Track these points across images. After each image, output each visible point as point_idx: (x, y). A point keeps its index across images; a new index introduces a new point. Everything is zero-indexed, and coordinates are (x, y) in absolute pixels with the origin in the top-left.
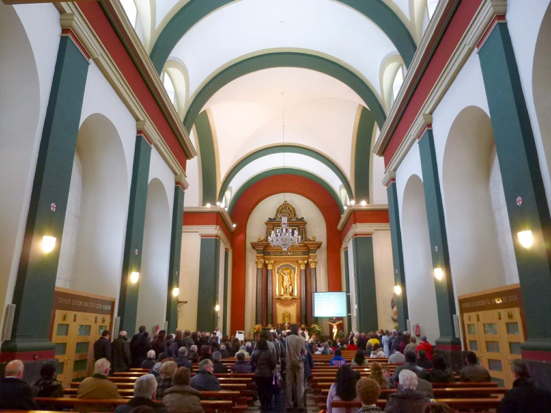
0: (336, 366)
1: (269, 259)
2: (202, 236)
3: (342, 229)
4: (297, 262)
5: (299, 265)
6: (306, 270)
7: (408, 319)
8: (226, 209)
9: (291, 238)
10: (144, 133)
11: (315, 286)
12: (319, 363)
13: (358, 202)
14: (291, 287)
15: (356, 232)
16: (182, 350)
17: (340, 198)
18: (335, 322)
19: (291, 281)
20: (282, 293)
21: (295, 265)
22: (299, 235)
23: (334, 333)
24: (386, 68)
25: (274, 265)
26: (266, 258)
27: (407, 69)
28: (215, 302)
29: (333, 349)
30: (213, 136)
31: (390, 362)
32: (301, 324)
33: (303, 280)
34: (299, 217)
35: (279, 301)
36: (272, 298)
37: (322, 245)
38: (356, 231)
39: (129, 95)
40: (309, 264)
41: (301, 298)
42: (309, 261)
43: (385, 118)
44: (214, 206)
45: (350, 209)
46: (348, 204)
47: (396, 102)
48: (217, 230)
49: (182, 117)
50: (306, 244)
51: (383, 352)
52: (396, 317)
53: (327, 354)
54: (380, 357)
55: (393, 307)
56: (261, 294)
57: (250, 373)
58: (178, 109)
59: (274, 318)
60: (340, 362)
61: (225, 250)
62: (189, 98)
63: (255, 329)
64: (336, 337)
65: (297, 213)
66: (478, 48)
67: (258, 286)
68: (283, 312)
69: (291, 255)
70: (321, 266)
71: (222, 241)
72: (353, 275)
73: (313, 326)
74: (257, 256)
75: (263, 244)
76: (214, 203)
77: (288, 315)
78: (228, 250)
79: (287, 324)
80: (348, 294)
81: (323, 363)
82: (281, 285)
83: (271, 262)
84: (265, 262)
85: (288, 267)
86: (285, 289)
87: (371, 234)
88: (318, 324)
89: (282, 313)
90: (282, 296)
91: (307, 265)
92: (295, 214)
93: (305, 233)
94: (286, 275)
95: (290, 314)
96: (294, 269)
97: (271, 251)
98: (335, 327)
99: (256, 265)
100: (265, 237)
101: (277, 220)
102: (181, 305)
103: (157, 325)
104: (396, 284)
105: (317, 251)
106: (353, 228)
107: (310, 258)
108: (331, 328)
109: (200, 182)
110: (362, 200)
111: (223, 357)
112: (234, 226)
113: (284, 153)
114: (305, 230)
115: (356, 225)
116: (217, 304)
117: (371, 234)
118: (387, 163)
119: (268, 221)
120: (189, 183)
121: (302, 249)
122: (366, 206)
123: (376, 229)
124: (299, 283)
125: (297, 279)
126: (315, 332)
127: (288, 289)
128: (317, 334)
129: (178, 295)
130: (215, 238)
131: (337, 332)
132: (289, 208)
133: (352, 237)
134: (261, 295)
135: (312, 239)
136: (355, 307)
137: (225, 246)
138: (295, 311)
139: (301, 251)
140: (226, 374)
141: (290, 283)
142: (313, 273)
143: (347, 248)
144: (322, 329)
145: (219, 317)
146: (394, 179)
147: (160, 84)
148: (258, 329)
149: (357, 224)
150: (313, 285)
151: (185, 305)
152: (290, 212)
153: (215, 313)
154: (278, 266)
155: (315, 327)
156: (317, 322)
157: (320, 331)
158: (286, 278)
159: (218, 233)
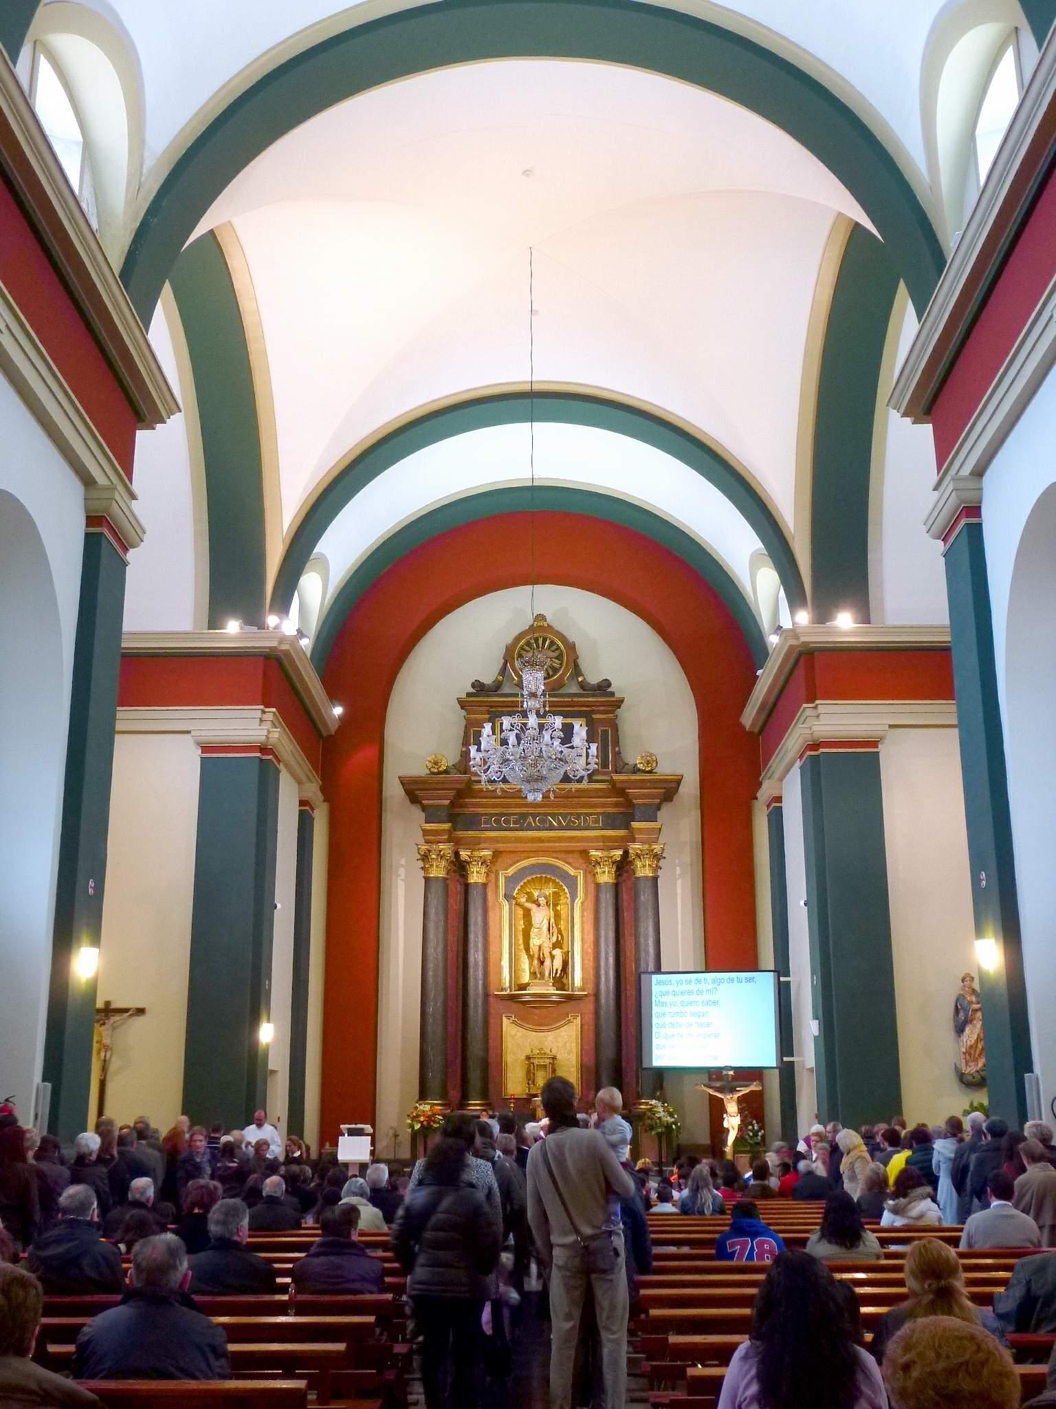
0: (744, 1262)
1: (474, 844)
2: (206, 749)
3: (760, 724)
4: (584, 853)
5: (590, 865)
6: (617, 886)
7: (1031, 1071)
8: (306, 643)
9: (562, 752)
10: (109, 522)
11: (651, 950)
12: (672, 1249)
13: (823, 615)
14: (557, 953)
15: (816, 735)
16: (70, 1196)
17: (753, 607)
18: (733, 1090)
19: (560, 932)
20: (526, 978)
21: (576, 868)
22: (590, 739)
23: (728, 1130)
25: (491, 865)
27: (1040, 46)
28: (255, 1008)
29: (726, 1196)
30: (252, 347)
31: (970, 1245)
33: (607, 924)
34: (593, 679)
35: (514, 1006)
36: (487, 995)
37: (683, 789)
38: (815, 728)
39: (59, 403)
40: (631, 863)
41: (597, 995)
42: (631, 851)
43: (939, 260)
44: (254, 629)
45: (794, 642)
46: (786, 623)
48: (267, 726)
49: (116, 248)
50: (618, 785)
51: (934, 1206)
52: (971, 1069)
53: (702, 1213)
54: (922, 1223)
55: (960, 1030)
56: (440, 980)
57: (371, 1293)
58: (99, 217)
59: (492, 1072)
60: (760, 1245)
61: (424, 835)
62: (145, 171)
64: (736, 1149)
65: (584, 664)
67: (431, 951)
68: (528, 1052)
69: (561, 828)
70: (678, 871)
71: (287, 766)
72: (802, 903)
73: (647, 1104)
74: (425, 832)
75: (452, 782)
76: (253, 618)
77: (548, 1061)
78: (313, 809)
80: (782, 979)
81: (685, 1250)
83: (482, 853)
84: (457, 854)
85: (546, 874)
86: (536, 962)
87: (874, 744)
88: (663, 1100)
90: (523, 987)
91: (623, 866)
92: (576, 666)
93: (616, 742)
94: (539, 905)
95: (554, 1058)
96: (572, 882)
97: (480, 810)
98: (732, 1107)
99: (422, 868)
100: (458, 758)
101: (506, 689)
102: (122, 1024)
103: (7, 1100)
104: (979, 932)
105: (663, 814)
106: (769, 775)
107: (634, 841)
108: (717, 1110)
109: (197, 533)
110: (838, 612)
111: (255, 1228)
112: (338, 711)
113: (538, 426)
115: (815, 708)
116: (264, 1018)
117: (874, 744)
118: (944, 448)
119: (469, 695)
120: (146, 526)
121: (604, 805)
122: (854, 633)
123: (892, 723)
124: (590, 937)
125: (582, 923)
126: (652, 1128)
127: (548, 963)
128: (660, 1135)
129: (97, 974)
130: (258, 755)
131: (740, 1129)
132: (552, 643)
133: (801, 757)
134: (441, 986)
135: (639, 766)
136: (809, 1028)
137: (300, 791)
138: (574, 1045)
139: (599, 810)
140: (267, 1298)
141: (554, 939)
142: (645, 897)
143: (779, 799)
144: (683, 1117)
145: (273, 1072)
146: (974, 510)
147: (19, 100)
148: (430, 1118)
149: (818, 702)
150: (647, 945)
151: (139, 1021)
152: (556, 658)
153: (256, 1053)
156: (661, 1087)
157: (674, 1126)
158: (540, 917)
159: (270, 736)
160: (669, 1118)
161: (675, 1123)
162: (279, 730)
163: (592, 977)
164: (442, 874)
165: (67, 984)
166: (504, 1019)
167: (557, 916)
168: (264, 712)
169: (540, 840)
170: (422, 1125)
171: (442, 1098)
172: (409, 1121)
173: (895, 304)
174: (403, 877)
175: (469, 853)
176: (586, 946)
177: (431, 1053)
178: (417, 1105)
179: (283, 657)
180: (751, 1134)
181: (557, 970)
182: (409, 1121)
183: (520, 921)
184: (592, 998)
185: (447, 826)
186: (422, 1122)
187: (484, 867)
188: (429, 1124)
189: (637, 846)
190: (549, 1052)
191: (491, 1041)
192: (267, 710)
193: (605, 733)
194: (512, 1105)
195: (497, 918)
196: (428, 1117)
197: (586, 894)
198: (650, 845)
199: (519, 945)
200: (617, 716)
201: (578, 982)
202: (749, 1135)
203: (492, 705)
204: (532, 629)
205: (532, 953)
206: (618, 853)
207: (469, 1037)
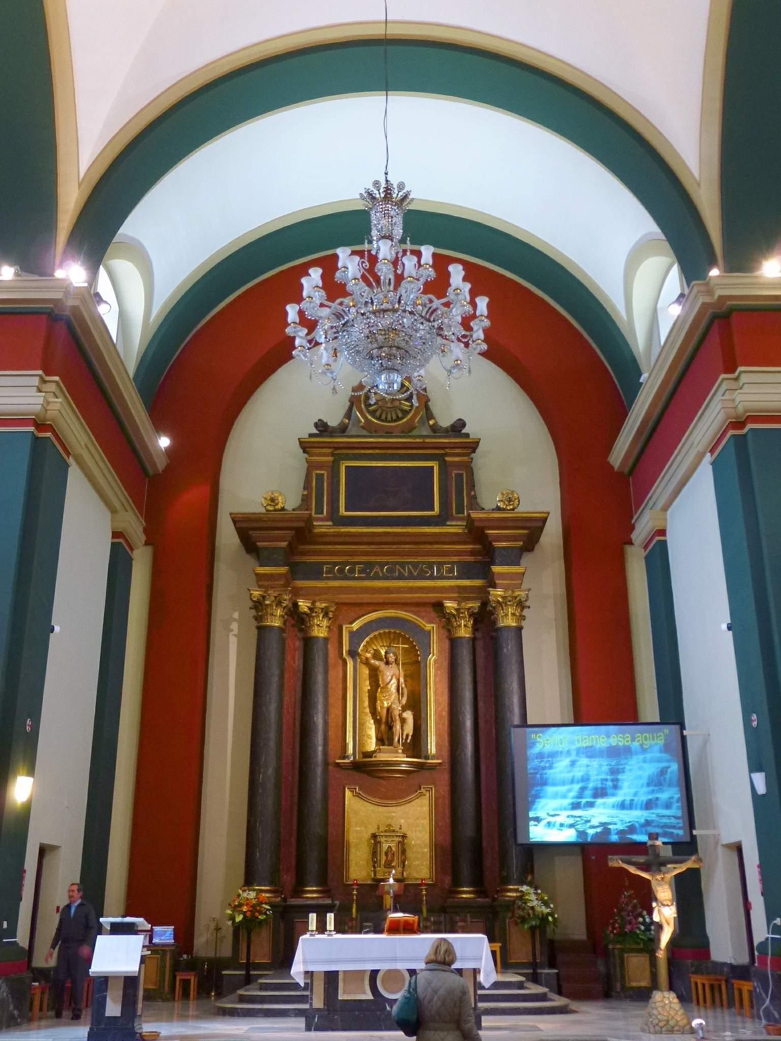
4: (438, 606)
5: (447, 621)
24: (642, 262)
26: (301, 588)
32: (457, 882)
34: (445, 421)
40: (492, 613)
45: (708, 300)
47: (666, 349)
50: (477, 524)
61: (113, 537)
63: (237, 908)
65: (436, 407)
66: (712, 455)
68: (372, 830)
72: (724, 627)
73: (516, 891)
79: (391, 881)
82: (367, 710)
86: (383, 727)
89: (367, 835)
92: (427, 408)
93: (472, 486)
95: (404, 836)
106: (651, 504)
107: (494, 586)
110: (766, 258)
112: (164, 442)
114: (471, 473)
119: (311, 435)
121: (459, 553)
126: (523, 920)
127: (398, 726)
128: (533, 929)
137: (112, 521)
139: (455, 559)
143: (662, 532)
148: (255, 908)
154: (356, 626)
155: (522, 897)
157: (550, 918)
161: (552, 914)
162: (60, 400)
165: (5, 803)
168: (44, 382)
169: (388, 590)
170: (245, 917)
171: (271, 883)
172: (229, 912)
174: (236, 631)
178: (241, 892)
179: (72, 318)
180: (642, 928)
181: (407, 736)
182: (229, 912)
183: (365, 681)
185: (283, 570)
188: (253, 915)
189: (499, 592)
190: (397, 829)
191: (331, 817)
192: (47, 378)
193: (459, 476)
194: (355, 892)
196: (253, 906)
198: (513, 592)
199: (364, 708)
200: (472, 459)
202: (640, 929)
203: (336, 447)
206: (475, 605)
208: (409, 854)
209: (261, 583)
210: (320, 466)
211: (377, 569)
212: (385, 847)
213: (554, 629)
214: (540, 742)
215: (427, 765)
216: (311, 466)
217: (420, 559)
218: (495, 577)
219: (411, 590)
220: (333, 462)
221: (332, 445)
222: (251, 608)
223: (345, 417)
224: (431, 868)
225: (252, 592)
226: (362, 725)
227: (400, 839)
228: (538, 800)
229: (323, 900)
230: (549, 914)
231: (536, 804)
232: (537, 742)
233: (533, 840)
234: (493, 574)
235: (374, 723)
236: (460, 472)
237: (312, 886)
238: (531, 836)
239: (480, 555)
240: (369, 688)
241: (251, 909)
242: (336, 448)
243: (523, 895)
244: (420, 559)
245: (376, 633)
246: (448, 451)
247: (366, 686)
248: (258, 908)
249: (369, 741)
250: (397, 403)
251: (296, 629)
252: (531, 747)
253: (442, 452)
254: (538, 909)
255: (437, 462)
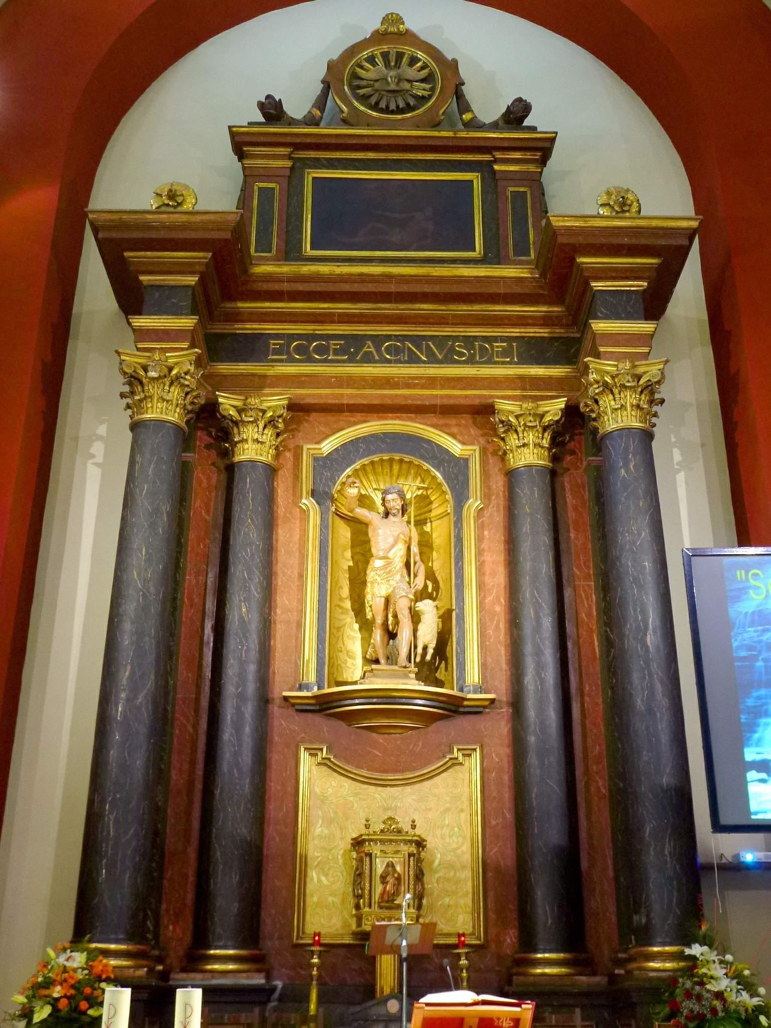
4: (485, 411)
19: (430, 575)
32: (528, 942)
41: (517, 704)
50: (561, 240)
59: (272, 880)
82: (348, 604)
86: (378, 635)
92: (459, 96)
95: (420, 844)
114: (540, 193)
119: (251, 124)
121: (522, 321)
139: (515, 332)
141: (420, 582)
160: (745, 995)
163: (504, 666)
164: (174, 416)
166: (304, 756)
167: (426, 545)
170: (55, 1009)
171: (130, 938)
173: (690, 253)
174: (100, 459)
175: (239, 404)
176: (488, 599)
177: (110, 819)
181: (425, 648)
183: (345, 550)
184: (506, 710)
186: (54, 1003)
187: (269, 432)
190: (406, 827)
194: (315, 960)
195: (296, 537)
196: (77, 986)
197: (487, 496)
199: (341, 599)
201: (473, 675)
204: (378, 37)
205: (369, 616)
206: (554, 408)
207: (217, 792)
208: (431, 882)
209: (140, 346)
210: (268, 175)
211: (369, 347)
212: (380, 867)
213: (701, 462)
214: (756, 588)
215: (466, 703)
216: (249, 176)
217: (447, 331)
218: (598, 341)
219: (432, 382)
220: (292, 169)
221: (289, 140)
222: (124, 384)
223: (314, 106)
224: (475, 910)
225: (122, 357)
226: (338, 629)
227: (413, 849)
228: (763, 721)
229: (248, 978)
230: (758, 1010)
231: (760, 729)
232: (750, 587)
233: (760, 816)
234: (594, 335)
235: (360, 629)
236: (522, 189)
237: (225, 947)
238: (753, 807)
239: (561, 326)
240: (351, 564)
241: (73, 992)
242: (298, 147)
243: (695, 966)
244: (447, 331)
245: (365, 461)
246: (498, 155)
247: (346, 560)
248: (88, 990)
249: (349, 661)
250: (407, 86)
251: (213, 453)
252: (737, 599)
253: (487, 157)
254: (732, 997)
255: (479, 175)
